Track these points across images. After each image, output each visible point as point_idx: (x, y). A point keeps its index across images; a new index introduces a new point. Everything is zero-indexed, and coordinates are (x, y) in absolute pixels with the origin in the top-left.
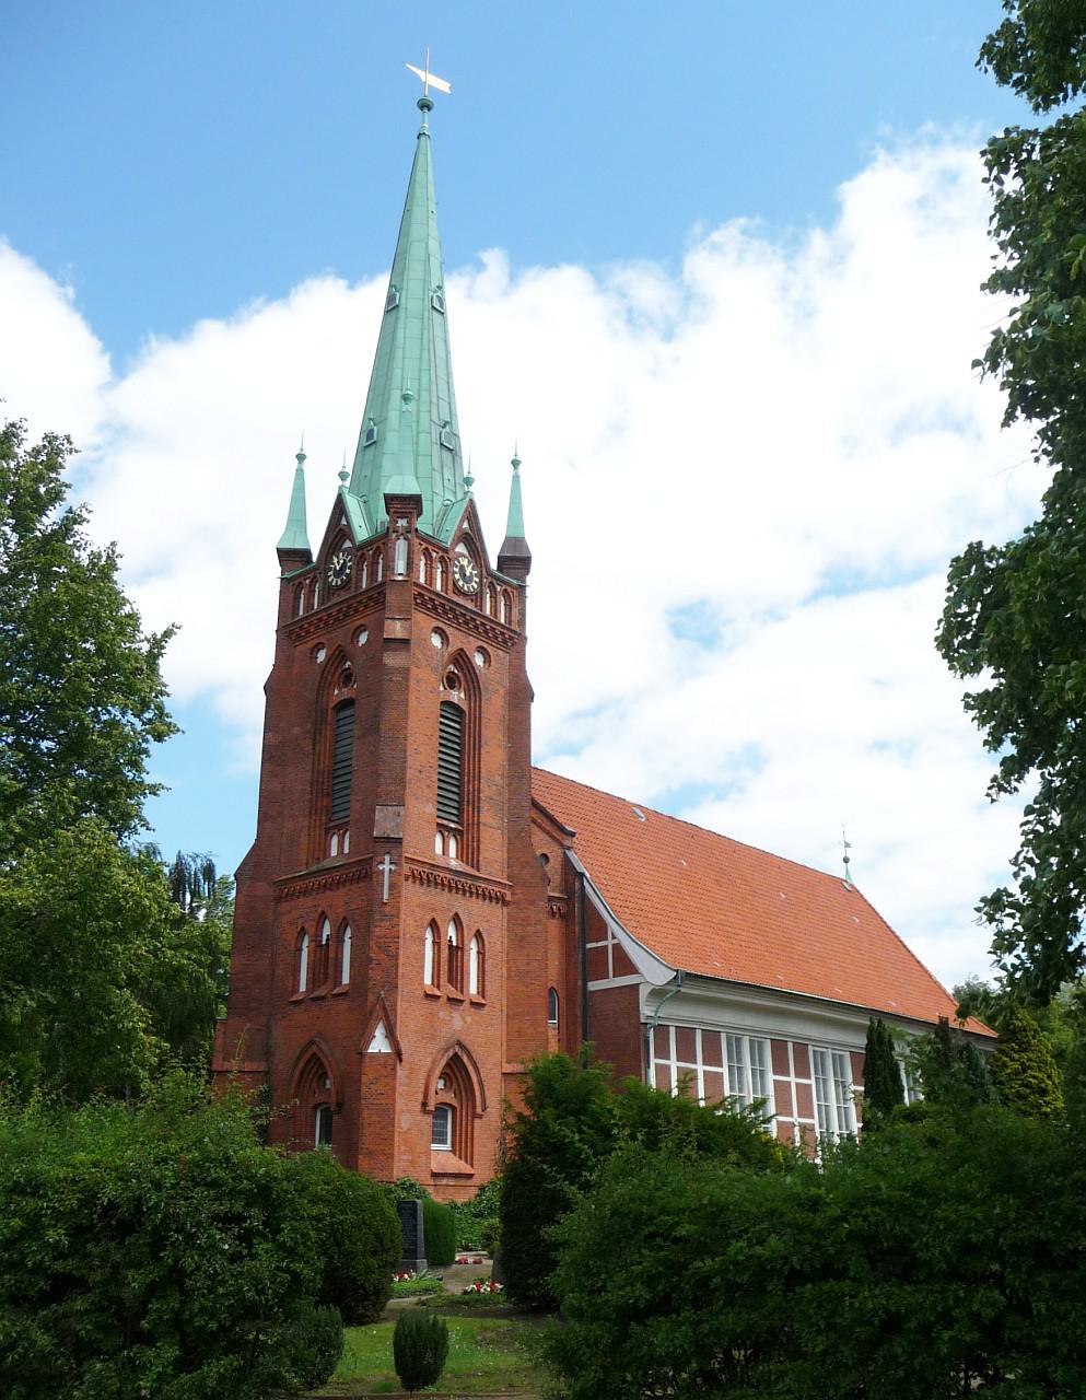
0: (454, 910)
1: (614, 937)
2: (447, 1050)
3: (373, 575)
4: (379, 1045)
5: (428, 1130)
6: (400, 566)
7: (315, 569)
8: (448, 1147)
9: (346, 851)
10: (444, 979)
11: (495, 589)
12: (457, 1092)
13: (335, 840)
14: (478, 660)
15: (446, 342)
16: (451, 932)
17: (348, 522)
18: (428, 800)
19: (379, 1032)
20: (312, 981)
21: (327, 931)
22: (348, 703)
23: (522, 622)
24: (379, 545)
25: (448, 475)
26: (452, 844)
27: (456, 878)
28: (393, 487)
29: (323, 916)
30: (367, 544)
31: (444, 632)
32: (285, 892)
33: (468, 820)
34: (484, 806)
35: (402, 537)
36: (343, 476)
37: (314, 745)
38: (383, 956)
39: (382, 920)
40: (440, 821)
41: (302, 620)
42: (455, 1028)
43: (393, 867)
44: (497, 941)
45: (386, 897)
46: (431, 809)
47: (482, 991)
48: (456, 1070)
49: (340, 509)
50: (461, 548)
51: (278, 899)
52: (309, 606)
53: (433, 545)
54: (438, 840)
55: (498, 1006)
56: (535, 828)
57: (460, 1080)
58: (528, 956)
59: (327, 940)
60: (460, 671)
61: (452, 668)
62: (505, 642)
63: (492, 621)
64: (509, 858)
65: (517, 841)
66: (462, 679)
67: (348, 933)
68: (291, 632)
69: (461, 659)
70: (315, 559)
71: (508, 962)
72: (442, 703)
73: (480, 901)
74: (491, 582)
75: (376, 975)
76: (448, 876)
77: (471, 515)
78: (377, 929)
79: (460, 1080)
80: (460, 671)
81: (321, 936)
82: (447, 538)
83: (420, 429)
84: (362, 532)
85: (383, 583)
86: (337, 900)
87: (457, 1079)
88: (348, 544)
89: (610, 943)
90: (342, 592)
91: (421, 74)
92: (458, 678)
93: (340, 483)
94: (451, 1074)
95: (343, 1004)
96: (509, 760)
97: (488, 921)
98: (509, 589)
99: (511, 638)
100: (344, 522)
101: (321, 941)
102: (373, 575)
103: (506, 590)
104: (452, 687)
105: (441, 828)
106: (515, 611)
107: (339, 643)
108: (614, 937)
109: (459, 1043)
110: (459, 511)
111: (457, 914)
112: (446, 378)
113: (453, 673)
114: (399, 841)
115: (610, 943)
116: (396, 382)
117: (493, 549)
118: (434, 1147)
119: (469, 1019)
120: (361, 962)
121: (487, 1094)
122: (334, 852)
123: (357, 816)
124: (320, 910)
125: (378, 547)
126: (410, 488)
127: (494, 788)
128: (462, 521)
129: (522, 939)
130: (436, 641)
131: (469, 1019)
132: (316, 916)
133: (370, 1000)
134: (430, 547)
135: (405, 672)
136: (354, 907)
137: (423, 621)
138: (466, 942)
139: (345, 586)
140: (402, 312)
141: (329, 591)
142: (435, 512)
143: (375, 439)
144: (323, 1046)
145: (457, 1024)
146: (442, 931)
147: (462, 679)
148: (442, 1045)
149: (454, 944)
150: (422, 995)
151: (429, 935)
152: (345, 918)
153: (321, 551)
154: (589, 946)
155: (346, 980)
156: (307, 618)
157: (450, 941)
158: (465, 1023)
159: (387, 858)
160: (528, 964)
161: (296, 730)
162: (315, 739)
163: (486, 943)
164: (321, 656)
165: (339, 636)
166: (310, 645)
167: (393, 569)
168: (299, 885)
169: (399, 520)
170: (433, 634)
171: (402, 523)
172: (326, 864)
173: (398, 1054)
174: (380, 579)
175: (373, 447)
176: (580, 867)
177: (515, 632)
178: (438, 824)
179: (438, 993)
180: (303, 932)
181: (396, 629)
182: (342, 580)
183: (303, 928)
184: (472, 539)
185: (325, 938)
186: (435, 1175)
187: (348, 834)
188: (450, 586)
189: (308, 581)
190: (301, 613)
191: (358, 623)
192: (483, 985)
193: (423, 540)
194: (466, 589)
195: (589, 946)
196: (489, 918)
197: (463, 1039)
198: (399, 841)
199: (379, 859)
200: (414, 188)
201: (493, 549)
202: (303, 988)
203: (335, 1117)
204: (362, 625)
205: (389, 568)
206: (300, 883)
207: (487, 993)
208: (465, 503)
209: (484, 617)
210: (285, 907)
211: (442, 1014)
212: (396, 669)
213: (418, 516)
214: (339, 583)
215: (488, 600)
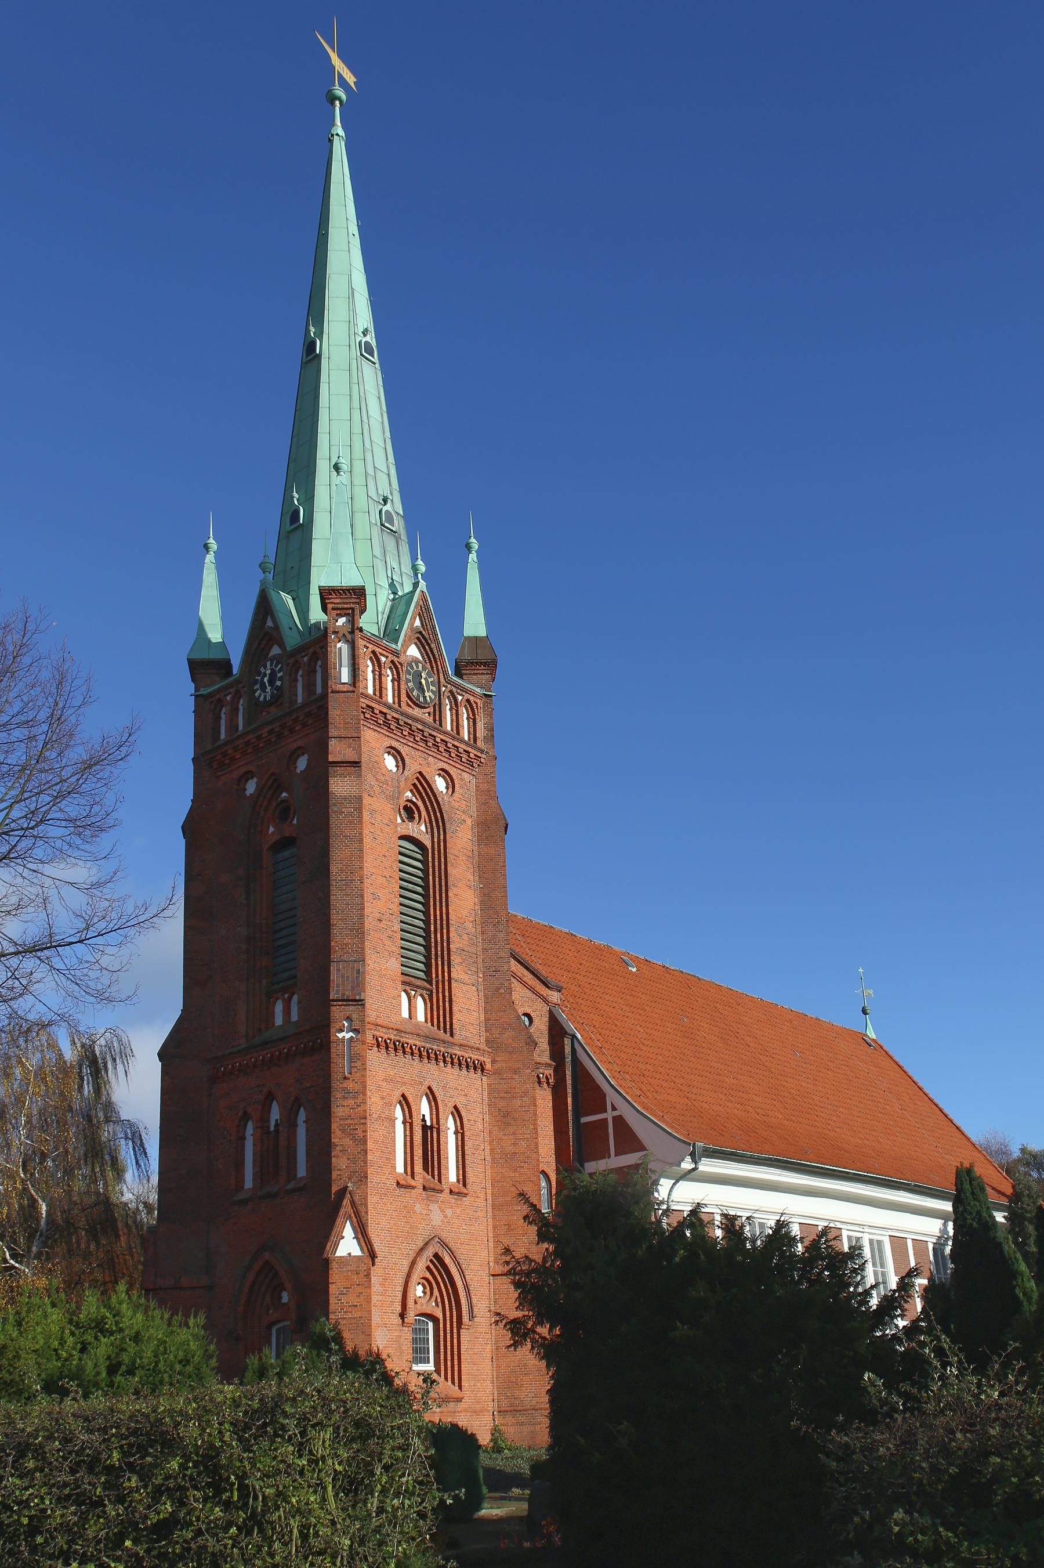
0: (427, 1084)
1: (614, 1108)
4: (348, 1245)
7: (237, 682)
9: (294, 1017)
13: (279, 1007)
16: (425, 1108)
19: (348, 1231)
20: (262, 1175)
21: (275, 1114)
22: (285, 843)
26: (420, 1003)
29: (270, 1097)
30: (300, 650)
33: (437, 976)
34: (455, 959)
36: (263, 567)
38: (347, 1141)
39: (344, 1098)
41: (226, 743)
42: (434, 1223)
44: (477, 1119)
47: (463, 1179)
48: (442, 1274)
52: (232, 727)
55: (482, 1195)
56: (515, 984)
58: (514, 1134)
59: (277, 1125)
60: (424, 802)
64: (487, 1020)
65: (496, 998)
66: (420, 803)
67: (302, 1115)
68: (210, 759)
69: (422, 786)
70: (235, 671)
71: (491, 1142)
75: (340, 1163)
78: (340, 1109)
80: (424, 802)
83: (355, 508)
88: (276, 650)
89: (609, 1115)
94: (431, 1278)
96: (482, 902)
97: (466, 1095)
98: (472, 699)
100: (270, 623)
101: (269, 1127)
108: (614, 1108)
109: (444, 1245)
113: (411, 801)
114: (360, 1003)
115: (609, 1115)
119: (449, 1212)
121: (474, 1301)
122: (279, 1021)
126: (351, 579)
127: (465, 937)
129: (507, 1115)
130: (390, 762)
131: (449, 1212)
133: (326, 1202)
134: (378, 650)
135: (358, 801)
139: (277, 699)
141: (256, 707)
142: (380, 610)
145: (436, 1217)
149: (428, 1123)
151: (398, 1113)
154: (584, 1120)
155: (302, 1171)
157: (424, 1120)
160: (515, 1144)
164: (251, 787)
166: (236, 775)
173: (372, 1255)
176: (571, 1027)
180: (246, 1117)
183: (245, 1113)
185: (273, 1123)
189: (228, 698)
191: (300, 743)
192: (464, 1172)
195: (584, 1120)
196: (467, 1090)
204: (299, 748)
207: (469, 1181)
211: (418, 1208)
212: (345, 799)
215: (448, 713)
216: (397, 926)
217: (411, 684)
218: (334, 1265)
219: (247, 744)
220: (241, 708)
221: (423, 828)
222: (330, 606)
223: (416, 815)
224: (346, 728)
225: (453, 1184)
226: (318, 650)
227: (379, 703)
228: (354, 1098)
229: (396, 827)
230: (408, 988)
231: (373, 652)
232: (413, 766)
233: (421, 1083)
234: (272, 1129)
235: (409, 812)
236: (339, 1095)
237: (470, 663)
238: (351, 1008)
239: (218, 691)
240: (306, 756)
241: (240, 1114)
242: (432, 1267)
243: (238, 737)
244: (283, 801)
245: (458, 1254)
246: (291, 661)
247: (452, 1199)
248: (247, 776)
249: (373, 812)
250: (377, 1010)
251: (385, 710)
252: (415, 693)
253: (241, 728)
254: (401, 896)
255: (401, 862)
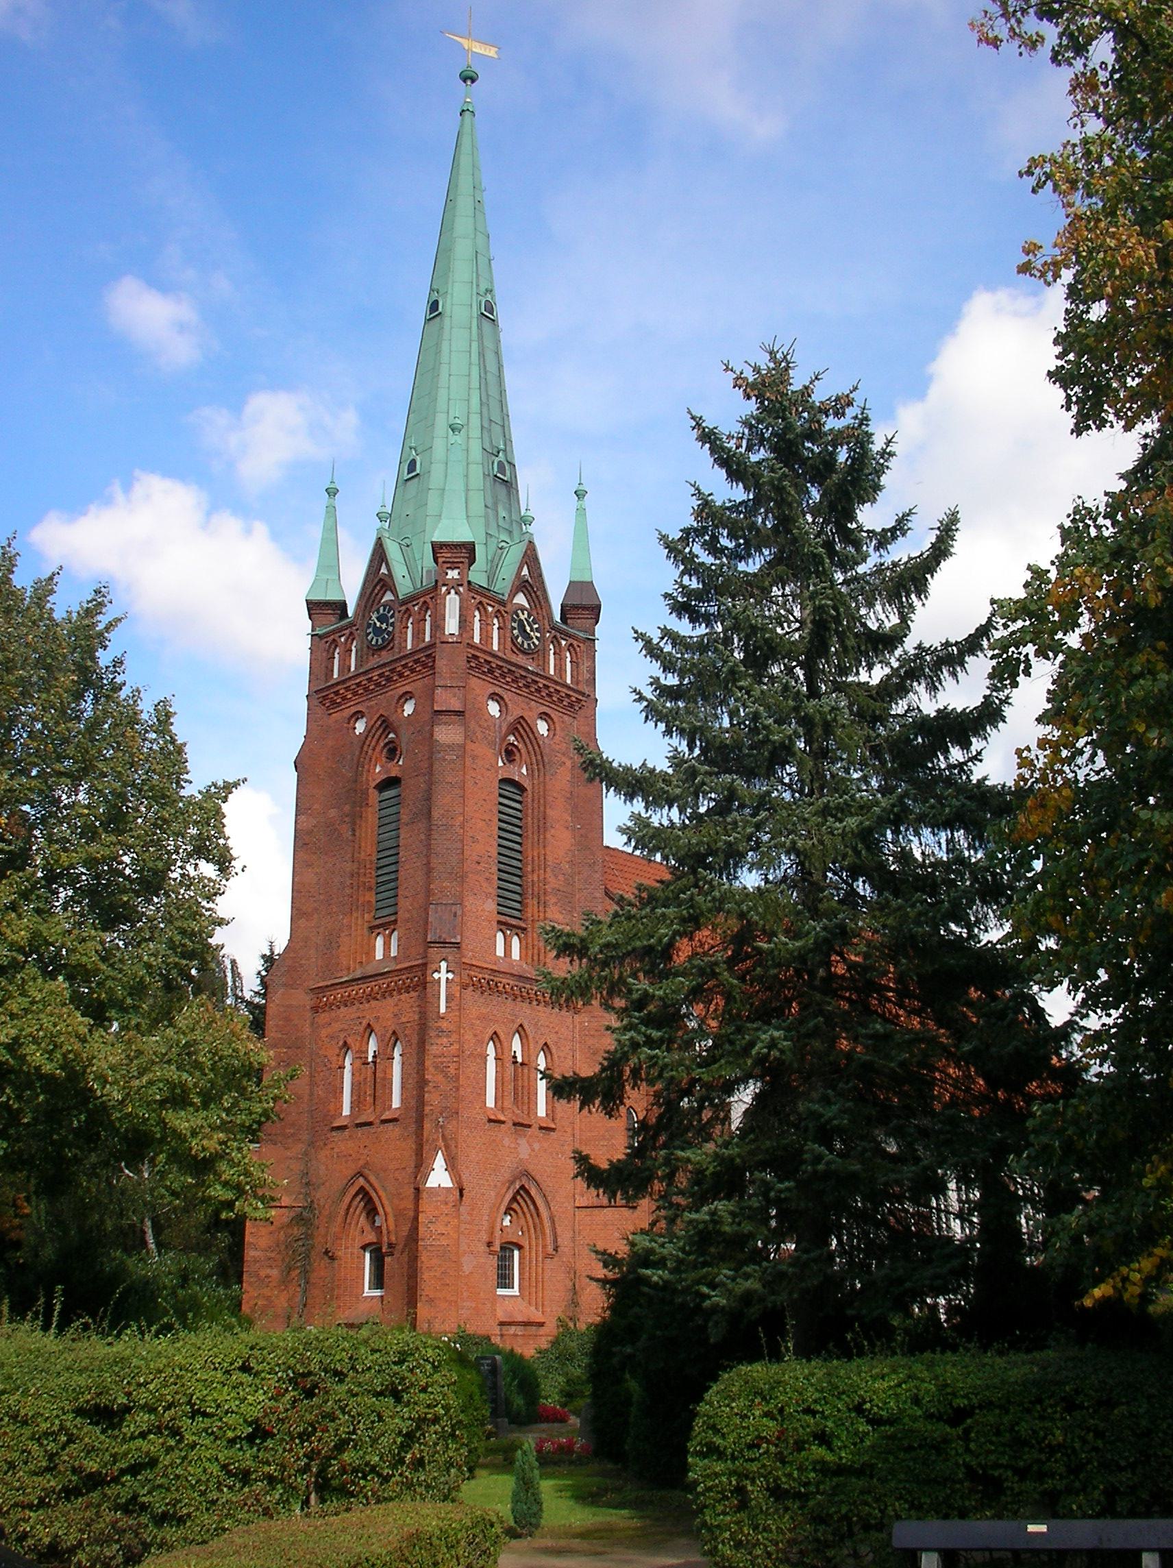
0: (519, 1021)
2: (512, 1182)
3: (419, 634)
5: (493, 1274)
6: (452, 626)
7: (352, 624)
8: (515, 1291)
9: (393, 953)
10: (508, 1103)
11: (560, 644)
12: (525, 1229)
13: (380, 942)
14: (542, 727)
15: (497, 353)
16: (516, 1045)
17: (389, 570)
18: (488, 895)
19: (440, 1162)
20: (356, 1103)
21: (372, 1046)
22: (391, 782)
23: (592, 681)
24: (427, 600)
25: (502, 513)
26: (515, 942)
27: (521, 984)
28: (442, 535)
30: (412, 599)
31: (502, 698)
32: (324, 999)
34: (552, 900)
35: (453, 591)
37: (354, 830)
39: (438, 1036)
40: (503, 918)
41: (338, 684)
42: (521, 1156)
43: (450, 976)
45: (443, 1010)
46: (491, 906)
49: (379, 555)
50: (520, 599)
51: (315, 1009)
52: (344, 667)
53: (486, 596)
54: (500, 936)
55: (569, 1130)
57: (528, 1215)
59: (374, 1057)
61: (512, 738)
62: (572, 706)
63: (556, 683)
68: (325, 696)
69: (521, 727)
70: (350, 612)
72: (502, 781)
73: (526, 1005)
74: (555, 637)
76: (512, 983)
77: (531, 557)
78: (435, 1047)
79: (528, 1215)
81: (367, 1051)
82: (502, 586)
83: (471, 459)
84: (404, 586)
85: (432, 645)
86: (387, 1011)
87: (524, 1213)
88: (388, 596)
90: (384, 653)
91: (465, 43)
92: (516, 747)
93: (379, 524)
95: (393, 1131)
98: (575, 643)
99: (579, 701)
100: (384, 570)
102: (419, 634)
103: (571, 645)
104: (511, 761)
105: (503, 926)
106: (584, 668)
107: (381, 712)
109: (527, 1174)
110: (515, 554)
111: (521, 1025)
112: (498, 397)
113: (513, 744)
116: (442, 403)
117: (556, 597)
118: (500, 1292)
119: (536, 1146)
120: (417, 1084)
121: (559, 1230)
122: (379, 955)
123: (407, 915)
124: (365, 1023)
125: (425, 602)
126: (462, 534)
127: (561, 877)
128: (520, 568)
130: (494, 709)
131: (536, 1146)
132: (361, 1029)
134: (484, 600)
136: (404, 1020)
137: (479, 686)
138: (533, 1058)
140: (447, 321)
143: (418, 471)
144: (372, 1179)
145: (524, 1150)
146: (505, 1044)
147: (523, 751)
148: (507, 1176)
149: (519, 1060)
150: (485, 1120)
151: (491, 1050)
152: (394, 1033)
153: (358, 605)
155: (396, 1103)
156: (344, 682)
157: (515, 1057)
158: (533, 1150)
159: (443, 965)
161: (333, 813)
162: (354, 823)
163: (555, 1056)
164: (360, 727)
165: (380, 703)
167: (444, 629)
168: (340, 993)
169: (449, 572)
170: (490, 702)
171: (453, 574)
172: (370, 970)
174: (427, 639)
175: (416, 480)
177: (583, 694)
178: (499, 922)
179: (502, 1118)
181: (447, 700)
182: (383, 639)
183: (345, 1042)
184: (532, 586)
185: (371, 1054)
186: (502, 1324)
187: (396, 933)
188: (509, 644)
189: (343, 639)
190: (335, 676)
191: (407, 688)
193: (477, 593)
194: (526, 646)
197: (530, 1168)
198: (457, 945)
199: (434, 967)
200: (458, 174)
201: (556, 597)
202: (346, 1111)
203: (388, 1259)
204: (407, 693)
205: (438, 626)
206: (356, 987)
207: (558, 1116)
208: (522, 548)
209: (546, 678)
210: (323, 1017)
211: (507, 1142)
212: (449, 746)
213: (471, 565)
214: (380, 641)
215: (552, 657)
216: (494, 869)
217: (515, 632)
218: (424, 1195)
219: (358, 685)
220: (354, 649)
221: (524, 771)
222: (440, 560)
223: (517, 757)
224: (451, 678)
225: (541, 1118)
226: (429, 600)
227: (485, 652)
228: (448, 1036)
229: (497, 772)
230: (503, 927)
231: (480, 603)
232: (515, 713)
233: (513, 1021)
234: (370, 1059)
235: (510, 754)
236: (432, 1034)
237: (576, 607)
238: (448, 950)
239: (333, 632)
240: (413, 701)
241: (341, 1043)
242: (505, 876)
243: (350, 678)
244: (391, 742)
245: (544, 1187)
246: (404, 608)
247: (541, 1134)
248: (358, 715)
249: (474, 758)
250: (472, 951)
251: (489, 659)
252: (520, 640)
253: (353, 669)
254: (500, 837)
255: (500, 804)
